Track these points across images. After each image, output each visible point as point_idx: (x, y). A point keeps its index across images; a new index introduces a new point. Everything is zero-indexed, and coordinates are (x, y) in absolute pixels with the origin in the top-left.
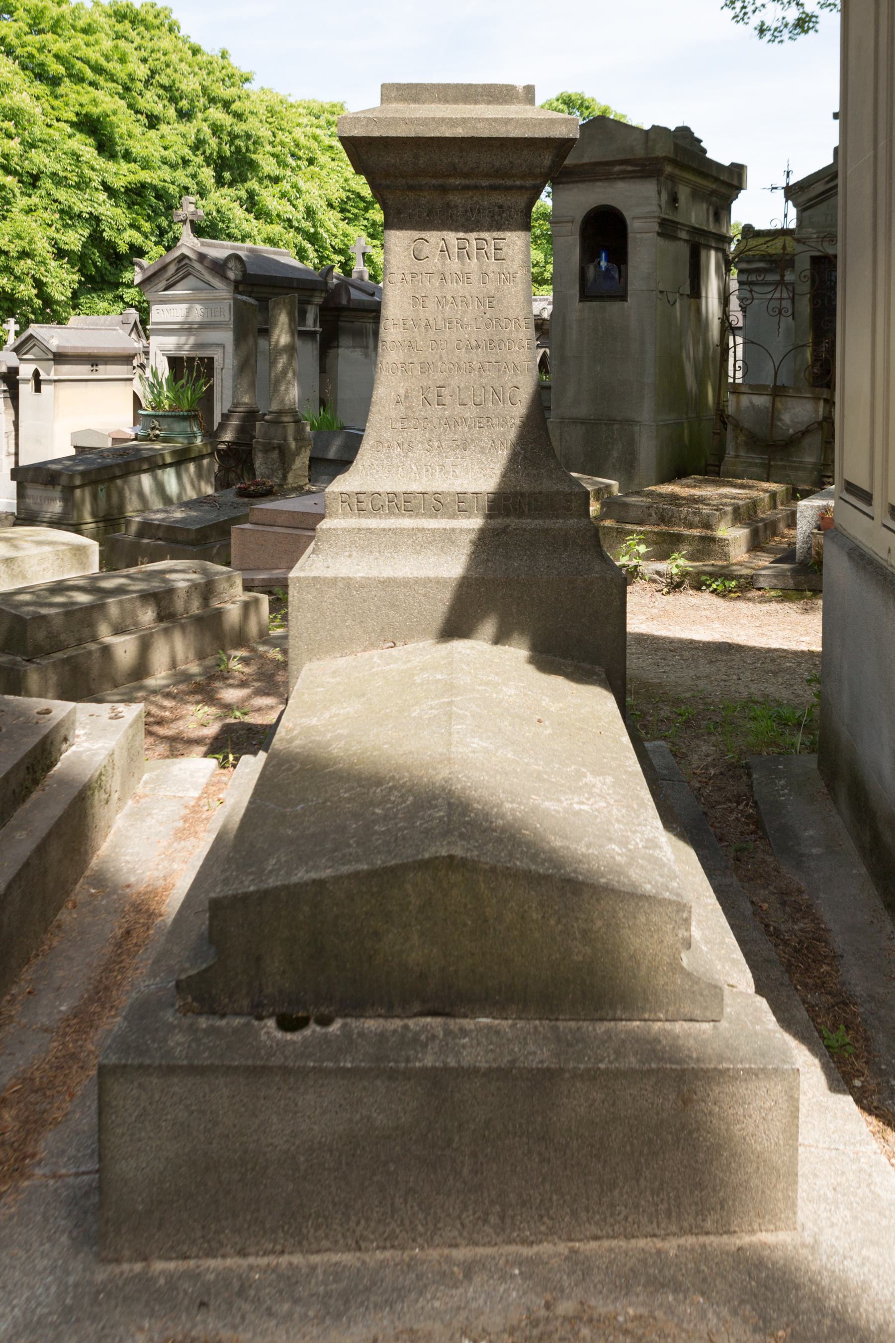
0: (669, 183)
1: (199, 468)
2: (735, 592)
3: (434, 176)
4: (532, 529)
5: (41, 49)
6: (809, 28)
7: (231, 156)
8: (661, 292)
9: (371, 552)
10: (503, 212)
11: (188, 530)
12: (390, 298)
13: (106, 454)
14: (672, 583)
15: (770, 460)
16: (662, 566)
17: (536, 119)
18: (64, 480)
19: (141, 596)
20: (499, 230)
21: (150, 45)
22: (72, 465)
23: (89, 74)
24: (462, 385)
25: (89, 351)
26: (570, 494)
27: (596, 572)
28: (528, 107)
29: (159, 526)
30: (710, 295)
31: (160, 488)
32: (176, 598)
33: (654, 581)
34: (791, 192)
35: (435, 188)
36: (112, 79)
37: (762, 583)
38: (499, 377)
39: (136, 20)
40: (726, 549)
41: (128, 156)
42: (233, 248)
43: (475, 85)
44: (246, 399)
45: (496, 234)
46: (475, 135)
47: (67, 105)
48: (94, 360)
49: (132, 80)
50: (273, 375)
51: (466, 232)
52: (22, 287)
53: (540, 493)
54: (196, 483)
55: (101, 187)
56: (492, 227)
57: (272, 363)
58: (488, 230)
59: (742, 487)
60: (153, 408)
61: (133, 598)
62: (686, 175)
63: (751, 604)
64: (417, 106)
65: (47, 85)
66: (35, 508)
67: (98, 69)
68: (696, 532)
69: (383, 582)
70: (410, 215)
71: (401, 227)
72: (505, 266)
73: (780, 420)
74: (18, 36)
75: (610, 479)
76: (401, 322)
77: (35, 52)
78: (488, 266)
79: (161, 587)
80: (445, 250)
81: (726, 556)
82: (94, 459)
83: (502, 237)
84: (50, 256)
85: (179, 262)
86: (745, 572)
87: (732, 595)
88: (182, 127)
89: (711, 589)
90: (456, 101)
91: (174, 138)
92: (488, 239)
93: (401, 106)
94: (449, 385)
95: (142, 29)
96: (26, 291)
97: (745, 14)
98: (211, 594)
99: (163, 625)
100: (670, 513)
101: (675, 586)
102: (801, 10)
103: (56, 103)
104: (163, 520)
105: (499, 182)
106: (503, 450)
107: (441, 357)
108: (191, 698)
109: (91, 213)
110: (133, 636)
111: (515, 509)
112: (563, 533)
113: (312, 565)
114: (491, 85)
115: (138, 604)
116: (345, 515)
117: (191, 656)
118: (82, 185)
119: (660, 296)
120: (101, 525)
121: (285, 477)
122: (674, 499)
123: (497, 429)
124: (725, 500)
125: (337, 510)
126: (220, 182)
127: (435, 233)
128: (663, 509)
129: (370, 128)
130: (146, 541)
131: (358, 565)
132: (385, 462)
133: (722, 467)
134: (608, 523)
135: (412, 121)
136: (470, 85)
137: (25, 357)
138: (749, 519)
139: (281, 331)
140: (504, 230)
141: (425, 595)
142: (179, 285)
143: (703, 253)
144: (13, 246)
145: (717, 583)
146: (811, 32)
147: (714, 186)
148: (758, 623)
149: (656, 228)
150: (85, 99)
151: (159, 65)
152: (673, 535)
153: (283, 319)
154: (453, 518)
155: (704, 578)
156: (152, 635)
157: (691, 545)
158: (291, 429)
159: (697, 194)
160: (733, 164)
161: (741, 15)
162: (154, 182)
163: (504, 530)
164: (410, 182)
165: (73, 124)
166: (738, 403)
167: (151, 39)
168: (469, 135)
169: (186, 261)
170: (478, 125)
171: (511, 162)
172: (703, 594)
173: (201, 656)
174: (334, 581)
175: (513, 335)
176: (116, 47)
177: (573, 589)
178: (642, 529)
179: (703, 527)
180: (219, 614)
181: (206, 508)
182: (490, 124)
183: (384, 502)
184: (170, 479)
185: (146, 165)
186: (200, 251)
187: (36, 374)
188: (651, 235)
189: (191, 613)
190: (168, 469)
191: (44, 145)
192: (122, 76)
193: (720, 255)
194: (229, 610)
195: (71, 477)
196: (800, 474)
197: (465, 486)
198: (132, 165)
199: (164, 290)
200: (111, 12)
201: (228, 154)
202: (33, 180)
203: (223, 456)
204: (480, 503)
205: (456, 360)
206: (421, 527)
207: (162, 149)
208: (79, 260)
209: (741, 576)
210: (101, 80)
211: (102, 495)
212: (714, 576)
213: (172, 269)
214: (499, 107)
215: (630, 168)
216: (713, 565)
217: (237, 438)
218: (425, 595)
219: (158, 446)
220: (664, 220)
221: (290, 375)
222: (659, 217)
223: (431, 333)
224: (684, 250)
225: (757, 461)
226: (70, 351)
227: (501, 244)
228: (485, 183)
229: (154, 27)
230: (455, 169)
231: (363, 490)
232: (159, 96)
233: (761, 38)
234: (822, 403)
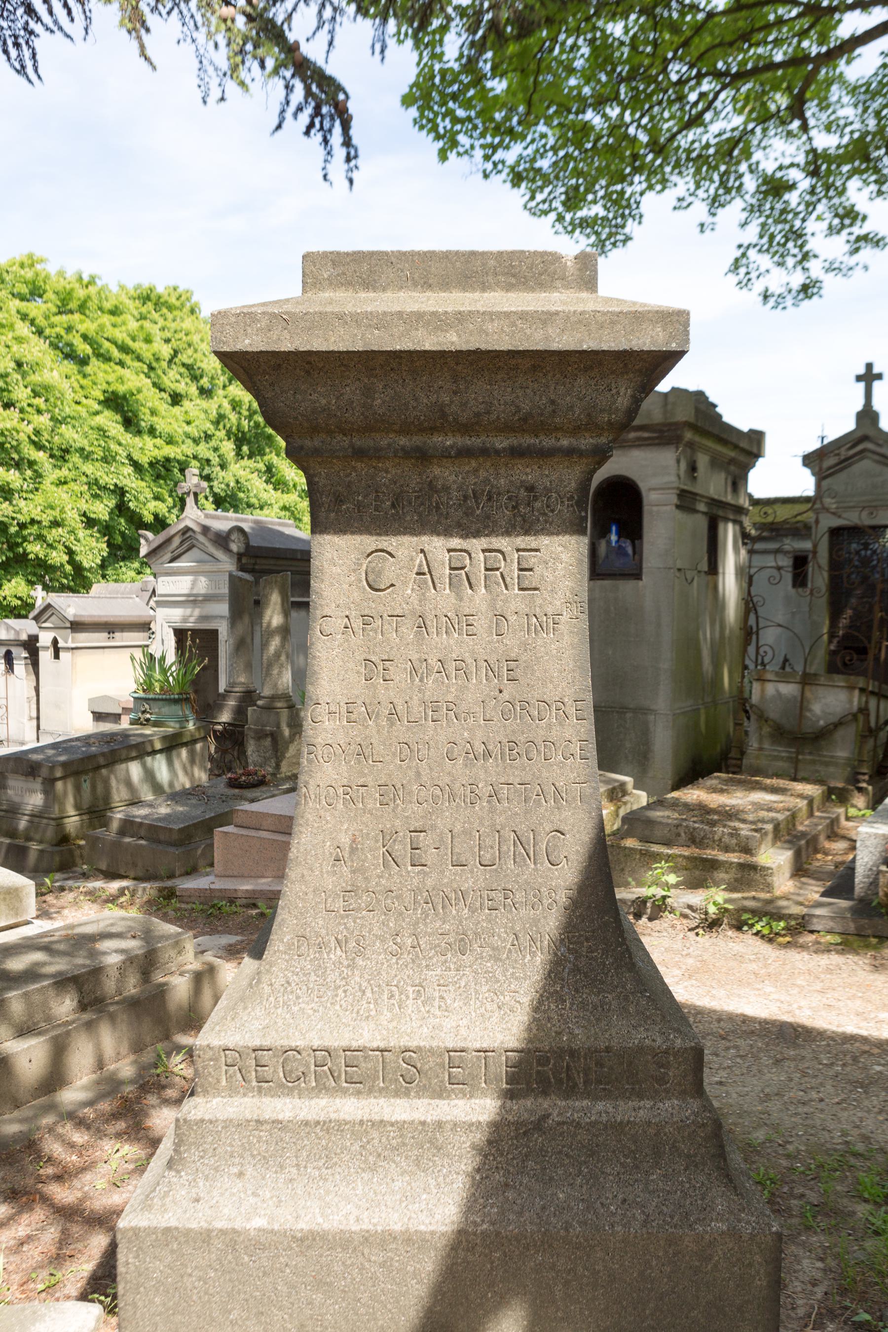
0: (688, 450)
1: (192, 754)
2: (784, 936)
3: (405, 429)
4: (593, 1124)
5: (69, 329)
6: (813, 294)
7: (250, 431)
8: (679, 570)
9: (282, 1167)
10: (536, 498)
11: (171, 830)
12: (323, 664)
13: (92, 740)
14: (706, 920)
15: (798, 753)
16: (696, 898)
17: (604, 314)
18: (44, 772)
19: (55, 983)
20: (527, 533)
21: (173, 326)
22: (54, 755)
23: (116, 353)
24: (458, 828)
25: (105, 619)
26: (666, 1052)
27: (720, 1217)
28: (584, 295)
29: (141, 824)
30: (727, 571)
31: (150, 776)
32: (104, 978)
33: (685, 916)
34: (809, 460)
35: (407, 454)
36: (139, 359)
37: (817, 925)
38: (526, 812)
39: (159, 303)
40: (769, 879)
41: (152, 431)
42: (237, 520)
43: (483, 254)
44: (242, 679)
45: (521, 541)
46: (483, 347)
47: (95, 383)
48: (110, 627)
49: (158, 360)
50: (265, 658)
51: (465, 536)
52: (54, 554)
53: (608, 1049)
54: (189, 768)
55: (127, 461)
56: (514, 527)
57: (265, 645)
58: (507, 533)
59: (774, 790)
60: (144, 691)
61: (43, 987)
62: (710, 444)
63: (805, 955)
64: (372, 295)
65: (75, 364)
66: (16, 799)
67: (124, 349)
68: (734, 858)
69: (302, 1240)
70: (359, 506)
71: (342, 529)
72: (539, 601)
73: (810, 710)
74: (47, 318)
75: (621, 774)
76: (344, 710)
77: (63, 333)
78: (506, 601)
79: (84, 966)
80: (426, 572)
81: (769, 887)
82: (79, 748)
83: (534, 545)
84: (81, 526)
85: (184, 534)
86: (796, 910)
87: (781, 939)
88: (204, 404)
89: (754, 931)
90: (445, 285)
91: (197, 413)
92: (507, 549)
93: (340, 295)
94: (434, 827)
95: (165, 310)
96: (58, 557)
97: (749, 280)
98: (152, 965)
99: (86, 1016)
100: (702, 834)
101: (712, 925)
102: (807, 275)
103: (84, 382)
104: (145, 817)
105: (528, 440)
106: (533, 954)
107: (418, 774)
108: (111, 1129)
109: (116, 485)
110: (42, 1039)
111: (560, 1081)
112: (652, 1131)
113: (166, 1194)
114: (513, 252)
115: (51, 992)
116: (232, 1091)
117: (124, 1049)
118: (108, 459)
119: (678, 574)
120: (85, 817)
121: (278, 766)
122: (703, 810)
123: (523, 912)
124: (763, 814)
125: (218, 1081)
126: (239, 455)
127: (407, 539)
128: (694, 829)
129: (274, 334)
130: (128, 840)
131: (255, 1194)
132: (313, 978)
133: (744, 761)
134: (630, 843)
135: (356, 319)
136: (473, 253)
137: (44, 625)
138: (789, 834)
139: (273, 612)
140: (536, 533)
141: (382, 1265)
142: (184, 557)
143: (721, 526)
144: (45, 516)
145: (761, 924)
146: (815, 298)
147: (732, 454)
148: (818, 986)
149: (674, 499)
150: (111, 378)
151: (182, 345)
152: (706, 860)
153: (275, 598)
154: (440, 1097)
155: (745, 916)
156: (68, 1033)
157: (727, 872)
158: (284, 714)
159: (716, 463)
161: (745, 281)
162: (178, 457)
163: (539, 1125)
164: (358, 442)
165: (100, 403)
166: (763, 691)
167: (174, 320)
168: (472, 347)
169: (190, 533)
170: (490, 327)
171: (553, 402)
172: (745, 936)
173: (137, 1048)
174: (206, 1237)
175: (554, 732)
176: (142, 327)
177: (675, 1255)
178: (670, 852)
179: (741, 851)
180: (161, 993)
181: (194, 801)
182: (513, 324)
183: (307, 1066)
184: (160, 766)
185: (170, 441)
186: (203, 523)
187: (55, 642)
188: (668, 508)
189: (126, 994)
190: (158, 756)
191: (73, 422)
192: (147, 356)
193: (737, 528)
194: (175, 986)
195: (52, 769)
196: (832, 769)
197: (463, 1032)
198: (158, 441)
199: (171, 562)
200: (135, 295)
201: (246, 429)
202: (61, 455)
203: (220, 737)
204: (492, 1069)
205: (447, 780)
206: (377, 1118)
207: (184, 425)
208: (107, 530)
209: (790, 916)
210: (127, 359)
211: (86, 786)
212: (758, 914)
213: (177, 541)
214: (529, 296)
215: (646, 435)
216: (754, 898)
217: (235, 719)
218: (382, 1265)
219: (148, 731)
220: (683, 491)
221: (283, 658)
222: (678, 488)
223: (400, 730)
224: (702, 523)
225: (783, 754)
226: (87, 620)
227: (532, 559)
228: (501, 443)
229: (176, 308)
230: (444, 415)
231: (266, 1043)
232: (181, 374)
233: (764, 304)
234: (857, 692)
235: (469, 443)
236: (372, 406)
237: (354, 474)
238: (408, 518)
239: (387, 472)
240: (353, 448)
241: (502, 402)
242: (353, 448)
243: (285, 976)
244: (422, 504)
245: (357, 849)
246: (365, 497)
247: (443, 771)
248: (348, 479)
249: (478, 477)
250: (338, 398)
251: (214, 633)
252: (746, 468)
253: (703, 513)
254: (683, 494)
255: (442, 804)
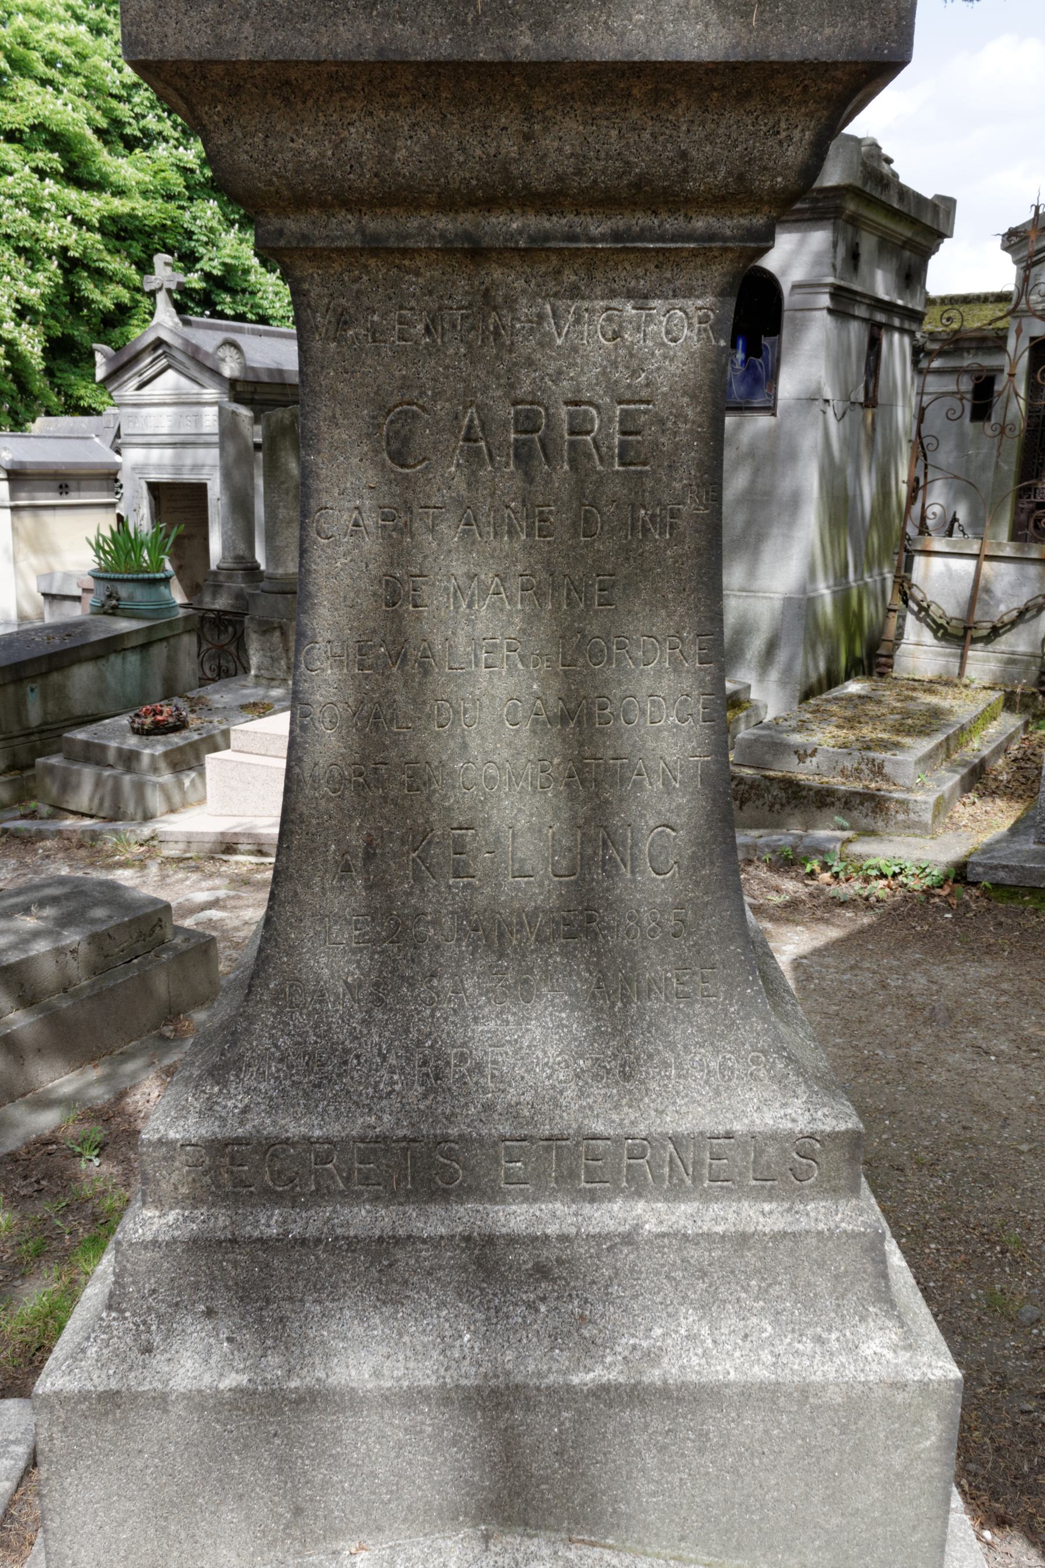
0: (850, 228)
12: (322, 581)
70: (374, 331)
159: (887, 246)
160: (937, 197)
222: (832, 285)
235: (547, 225)
236: (392, 161)
237: (365, 278)
238: (451, 351)
239: (417, 274)
240: (363, 233)
241: (603, 155)
242: (363, 233)
243: (272, 1036)
244: (473, 328)
245: (375, 854)
246: (383, 317)
247: (500, 741)
248: (355, 287)
249: (560, 283)
250: (336, 147)
251: (199, 490)
252: (926, 252)
253: (864, 320)
254: (839, 293)
255: (499, 789)
